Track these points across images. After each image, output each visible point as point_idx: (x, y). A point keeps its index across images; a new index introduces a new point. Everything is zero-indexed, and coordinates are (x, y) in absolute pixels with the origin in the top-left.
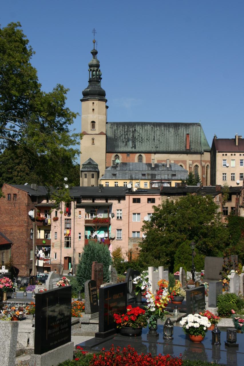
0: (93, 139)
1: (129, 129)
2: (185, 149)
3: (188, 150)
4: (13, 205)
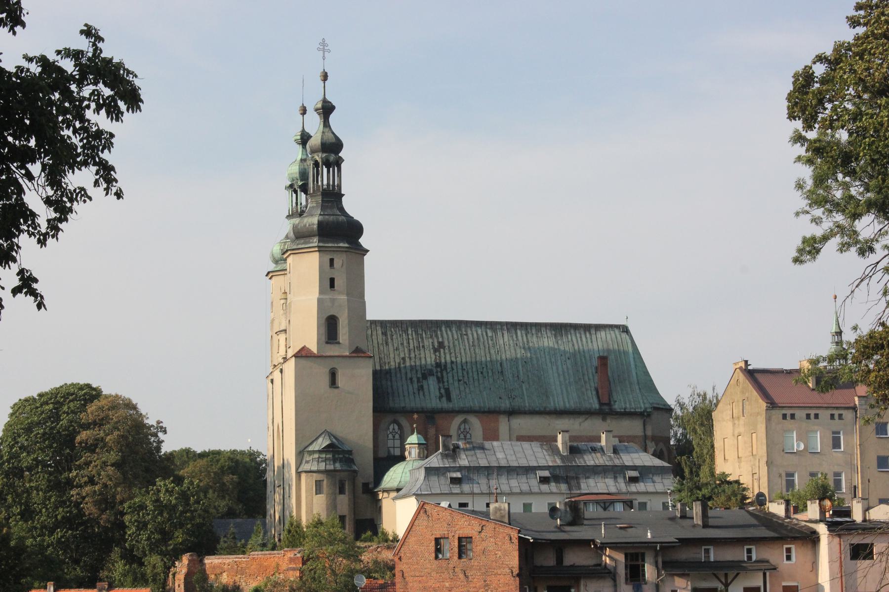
0: (333, 375)
1: (423, 342)
2: (596, 401)
3: (605, 404)
4: (461, 576)
